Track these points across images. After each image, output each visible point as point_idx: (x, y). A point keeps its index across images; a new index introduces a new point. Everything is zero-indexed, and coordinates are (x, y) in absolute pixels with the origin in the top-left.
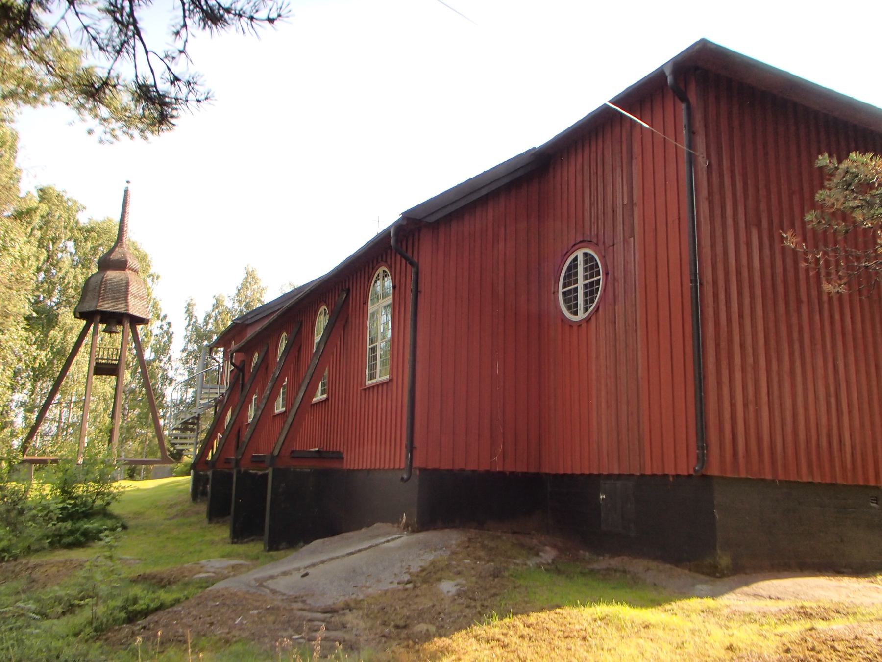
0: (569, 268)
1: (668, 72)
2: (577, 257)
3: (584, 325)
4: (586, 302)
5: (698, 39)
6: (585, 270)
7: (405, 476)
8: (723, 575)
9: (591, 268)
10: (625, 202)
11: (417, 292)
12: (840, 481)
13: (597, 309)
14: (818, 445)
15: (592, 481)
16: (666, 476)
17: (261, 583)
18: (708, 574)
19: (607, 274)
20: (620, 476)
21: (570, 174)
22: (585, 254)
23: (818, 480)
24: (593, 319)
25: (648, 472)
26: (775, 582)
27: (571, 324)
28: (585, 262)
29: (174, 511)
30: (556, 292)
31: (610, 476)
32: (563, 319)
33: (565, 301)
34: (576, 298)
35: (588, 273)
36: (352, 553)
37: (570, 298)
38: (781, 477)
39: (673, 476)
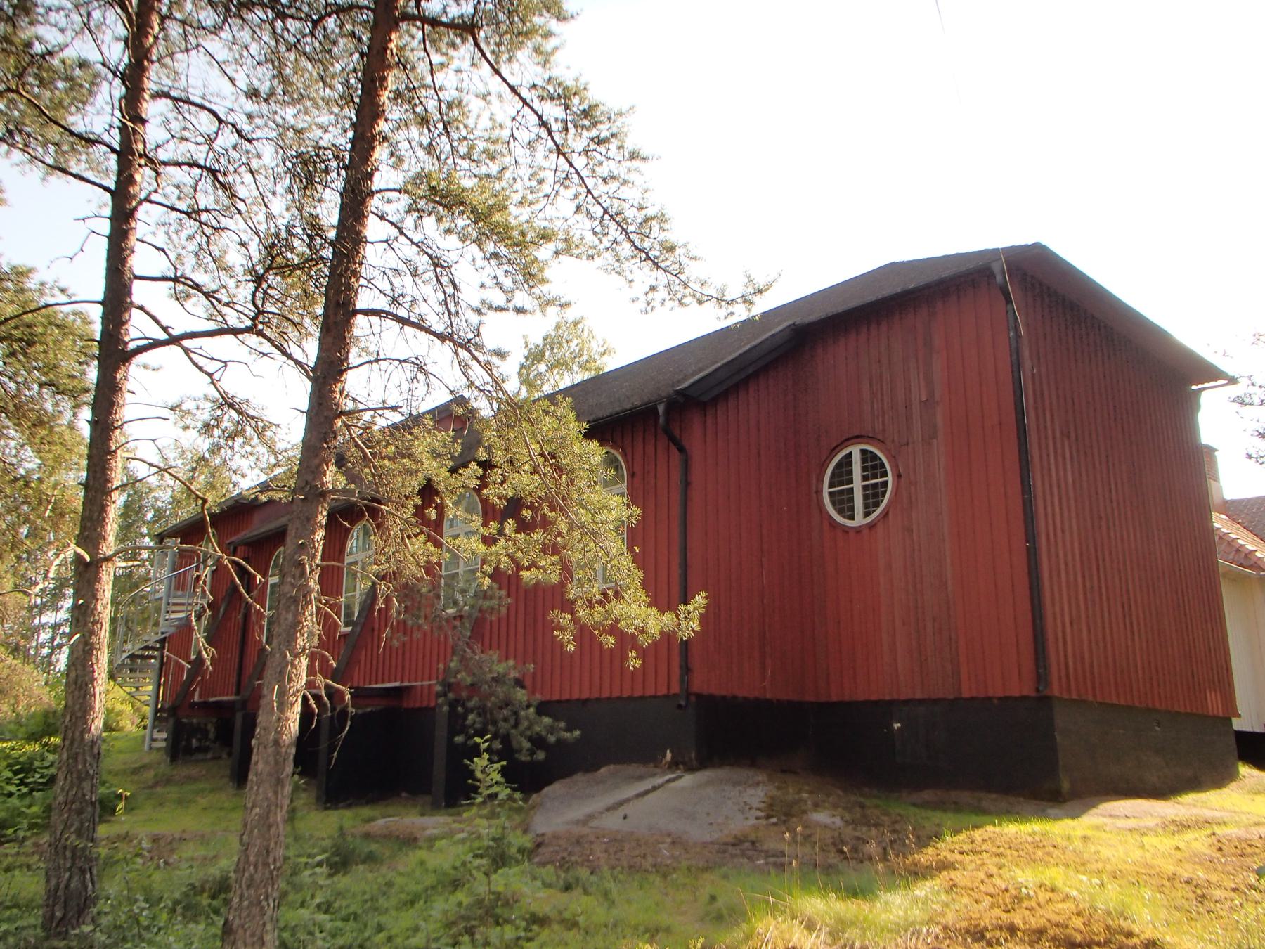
0: (839, 465)
1: (996, 268)
2: (850, 454)
3: (866, 532)
4: (866, 506)
5: (1030, 241)
6: (864, 469)
7: (683, 703)
8: (1065, 801)
9: (872, 466)
10: (924, 398)
11: (687, 484)
12: (1137, 704)
13: (885, 515)
14: (1092, 673)
15: (884, 709)
16: (989, 699)
17: (585, 822)
18: (1049, 800)
19: (899, 476)
20: (921, 701)
21: (837, 360)
22: (863, 452)
23: (1122, 702)
24: (880, 529)
25: (966, 695)
26: (1038, 826)
27: (846, 530)
28: (864, 460)
29: (149, 775)
30: (819, 492)
31: (907, 702)
32: (833, 524)
33: (833, 503)
34: (852, 500)
35: (869, 473)
36: (647, 792)
37: (844, 503)
38: (1099, 699)
39: (1000, 699)
